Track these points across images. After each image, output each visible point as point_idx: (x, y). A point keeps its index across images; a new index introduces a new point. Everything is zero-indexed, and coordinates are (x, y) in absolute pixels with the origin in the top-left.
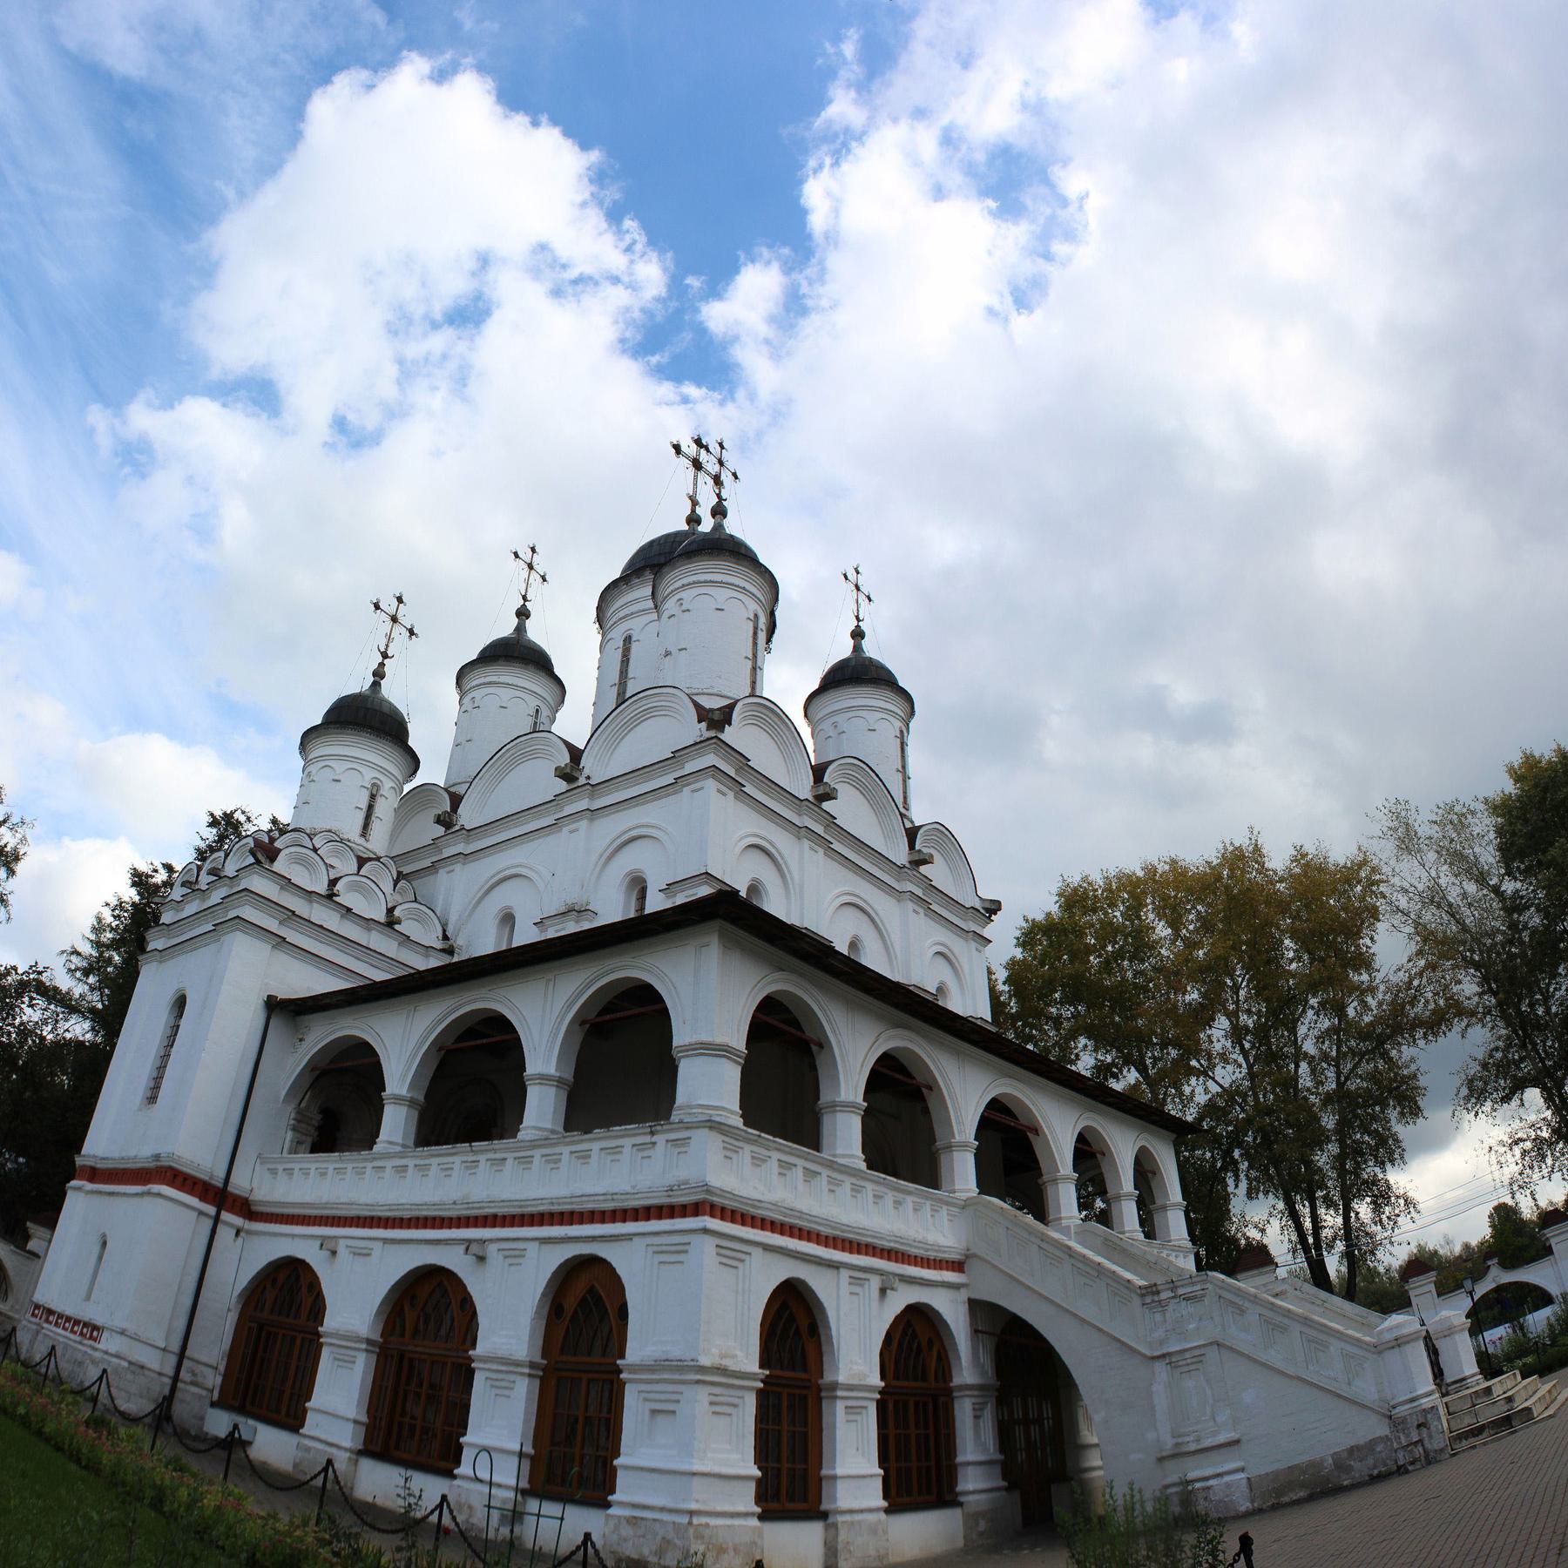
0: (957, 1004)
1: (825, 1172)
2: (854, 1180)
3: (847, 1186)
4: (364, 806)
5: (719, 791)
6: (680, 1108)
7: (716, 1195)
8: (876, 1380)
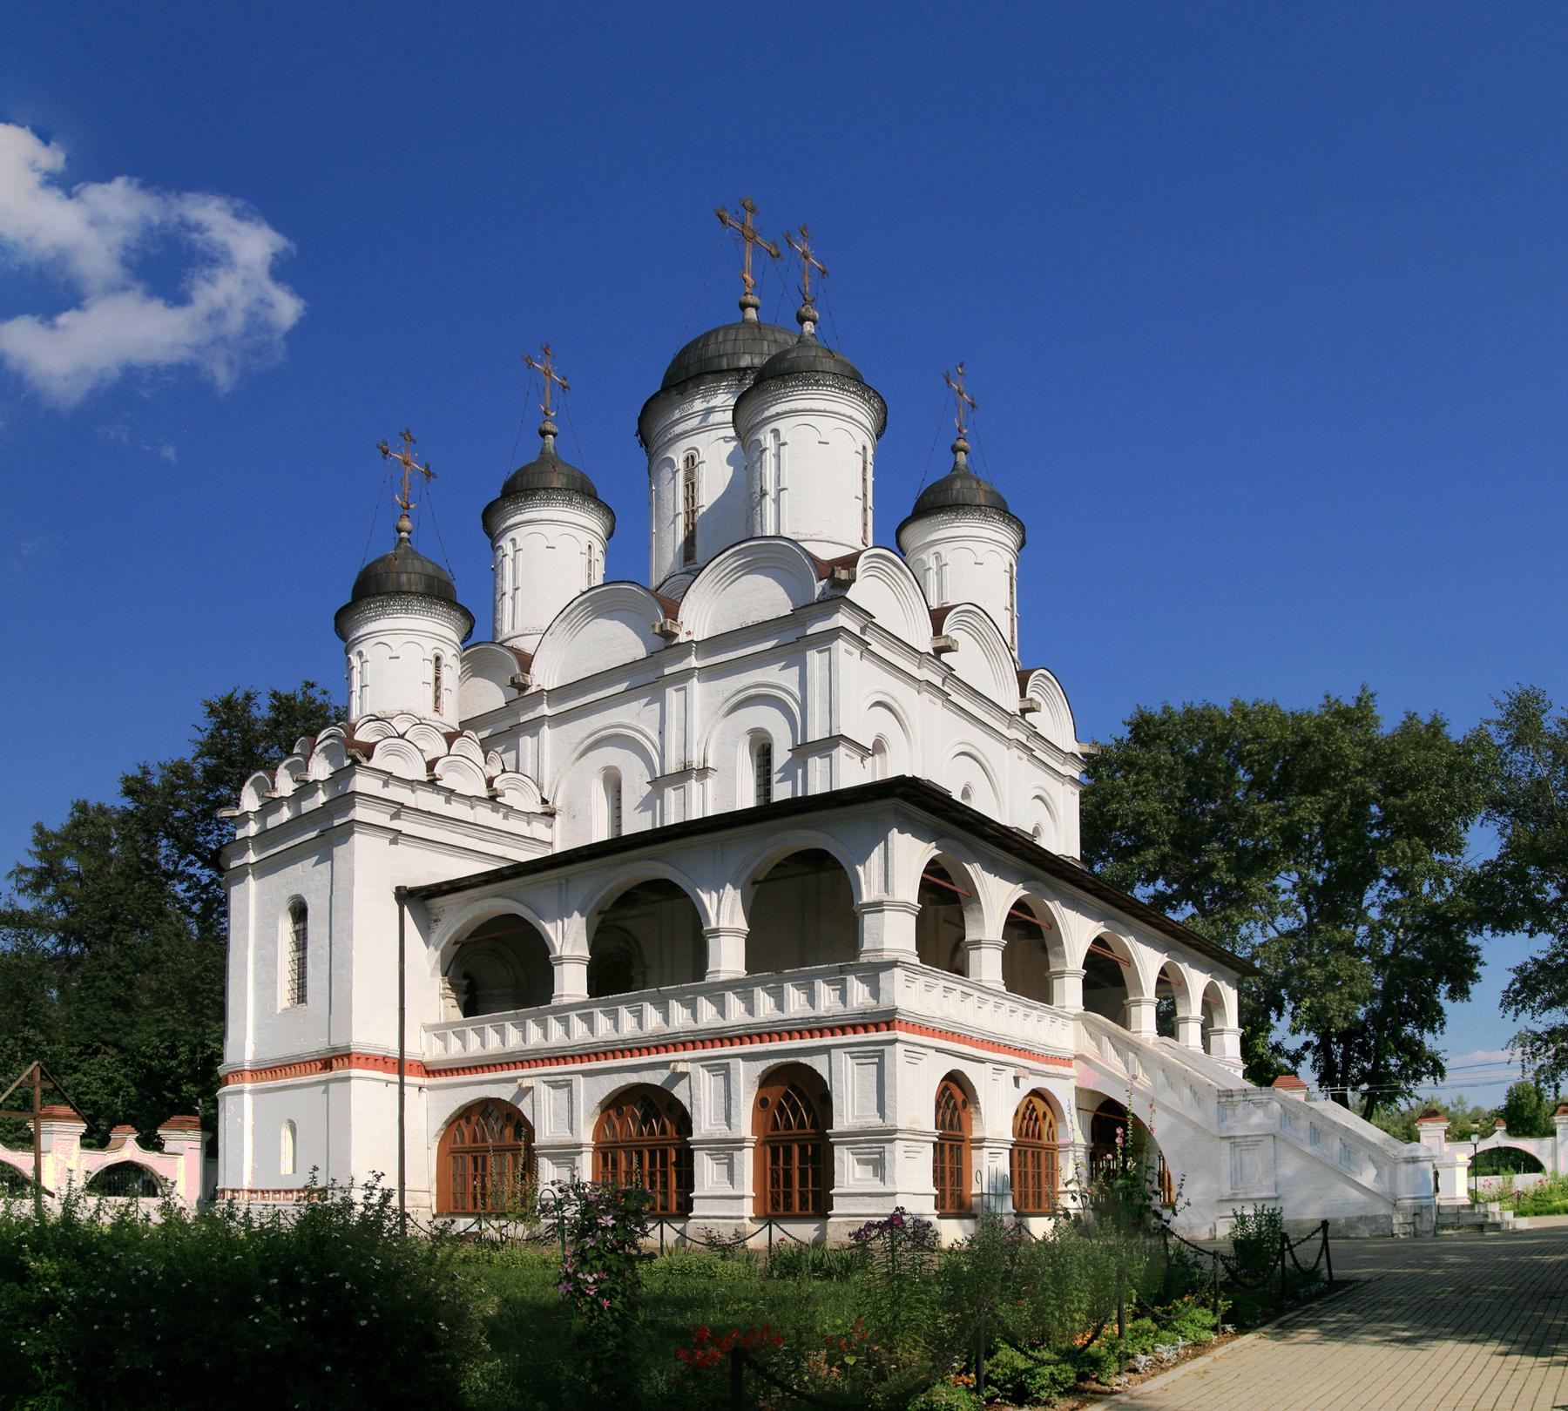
1: (976, 994)
2: (996, 999)
4: (431, 679)
5: (846, 651)
8: (1010, 1137)
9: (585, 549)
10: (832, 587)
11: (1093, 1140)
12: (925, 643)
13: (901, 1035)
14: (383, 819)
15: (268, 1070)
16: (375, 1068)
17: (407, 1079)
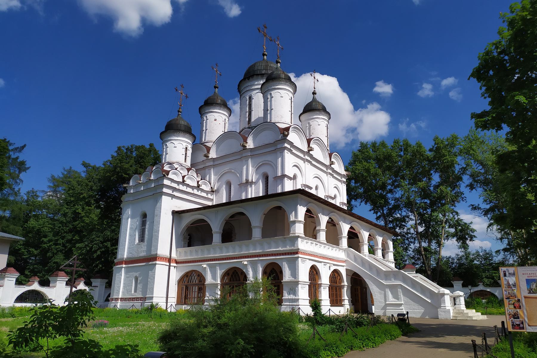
1: (319, 244)
4: (184, 153)
5: (287, 153)
9: (224, 120)
10: (283, 136)
14: (170, 191)
15: (129, 261)
16: (163, 261)
17: (172, 264)
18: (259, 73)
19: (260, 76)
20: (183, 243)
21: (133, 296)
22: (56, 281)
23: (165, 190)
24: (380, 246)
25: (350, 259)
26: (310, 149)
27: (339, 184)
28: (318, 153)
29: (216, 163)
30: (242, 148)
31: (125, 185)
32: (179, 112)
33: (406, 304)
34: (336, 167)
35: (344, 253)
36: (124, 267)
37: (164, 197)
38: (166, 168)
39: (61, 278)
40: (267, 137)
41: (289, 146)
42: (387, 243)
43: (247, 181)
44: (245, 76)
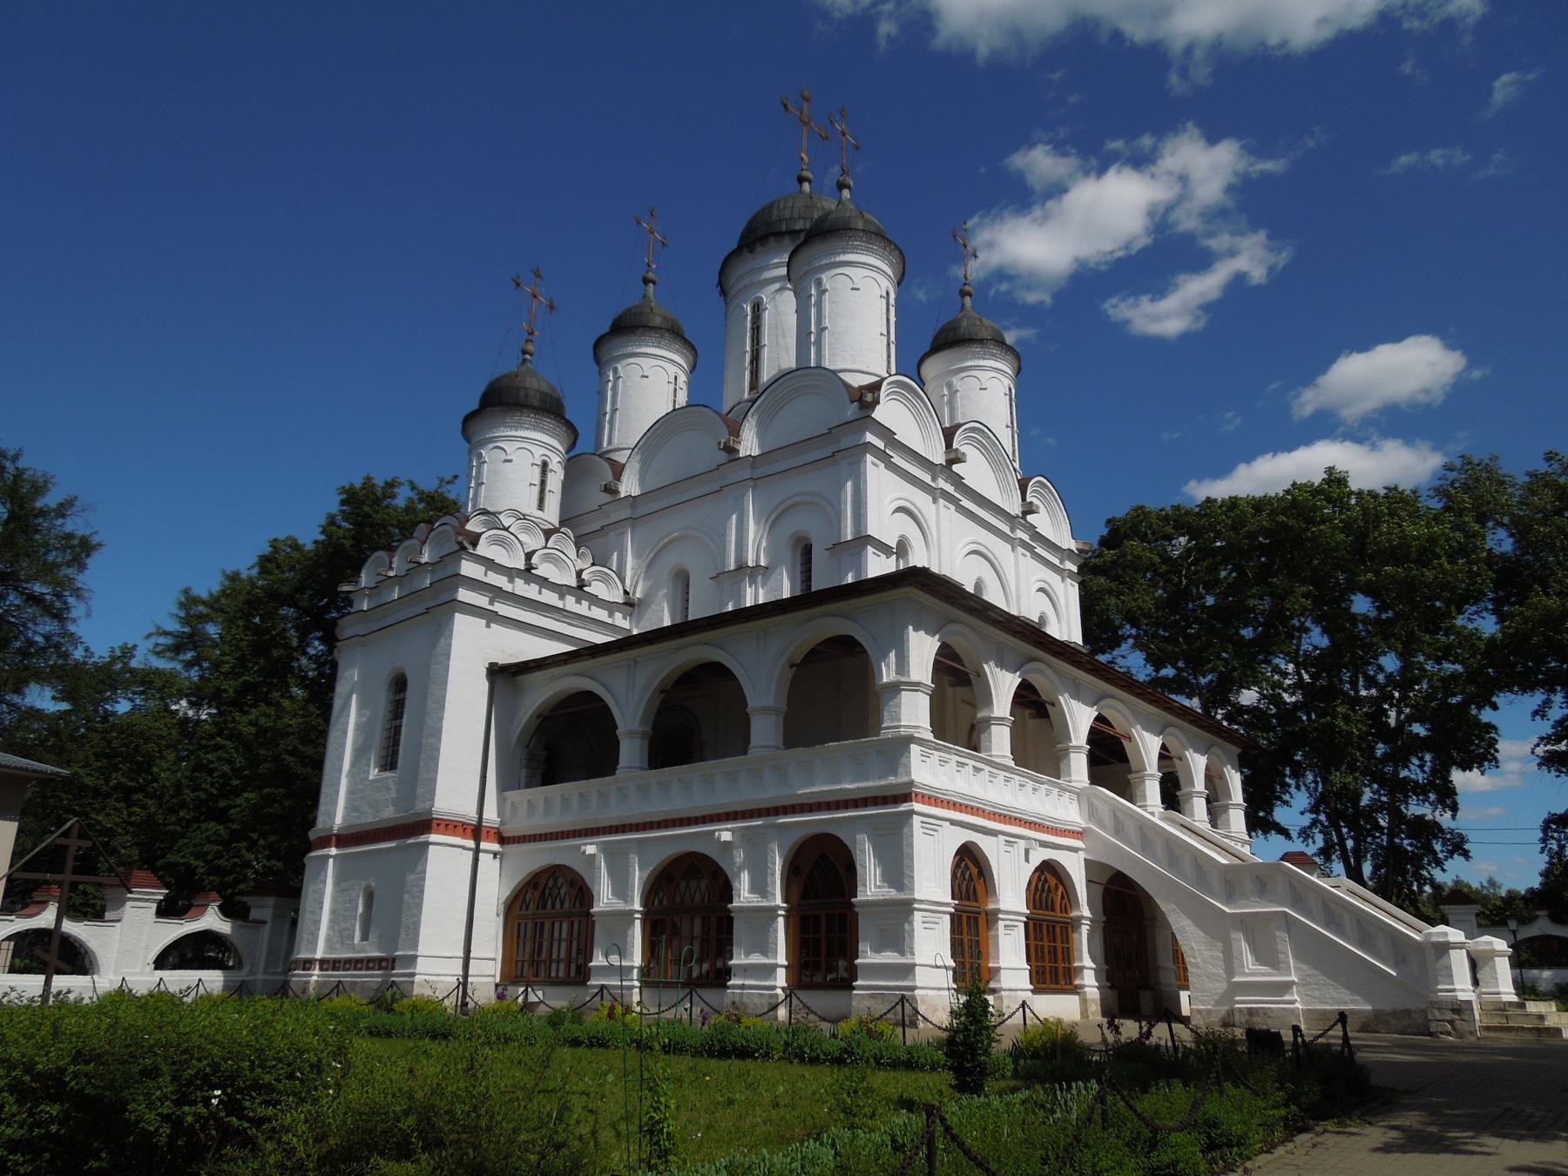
0: (1054, 630)
1: (987, 768)
2: (1006, 774)
3: (1001, 778)
4: (537, 481)
5: (873, 463)
6: (754, 747)
7: (919, 788)
9: (673, 380)
11: (1105, 913)
12: (938, 456)
13: (917, 806)
14: (481, 600)
15: (344, 840)
16: (454, 834)
17: (483, 845)
18: (784, 228)
19: (787, 238)
20: (524, 772)
21: (358, 952)
22: (122, 902)
23: (464, 595)
24: (1199, 784)
25: (1101, 825)
26: (954, 458)
27: (1054, 579)
28: (976, 471)
29: (642, 510)
30: (723, 457)
31: (346, 588)
32: (524, 352)
33: (1304, 983)
34: (1040, 520)
35: (1075, 803)
36: (334, 857)
37: (459, 618)
38: (472, 526)
39: (139, 893)
40: (805, 417)
41: (880, 444)
42: (1222, 777)
43: (741, 567)
44: (741, 239)
